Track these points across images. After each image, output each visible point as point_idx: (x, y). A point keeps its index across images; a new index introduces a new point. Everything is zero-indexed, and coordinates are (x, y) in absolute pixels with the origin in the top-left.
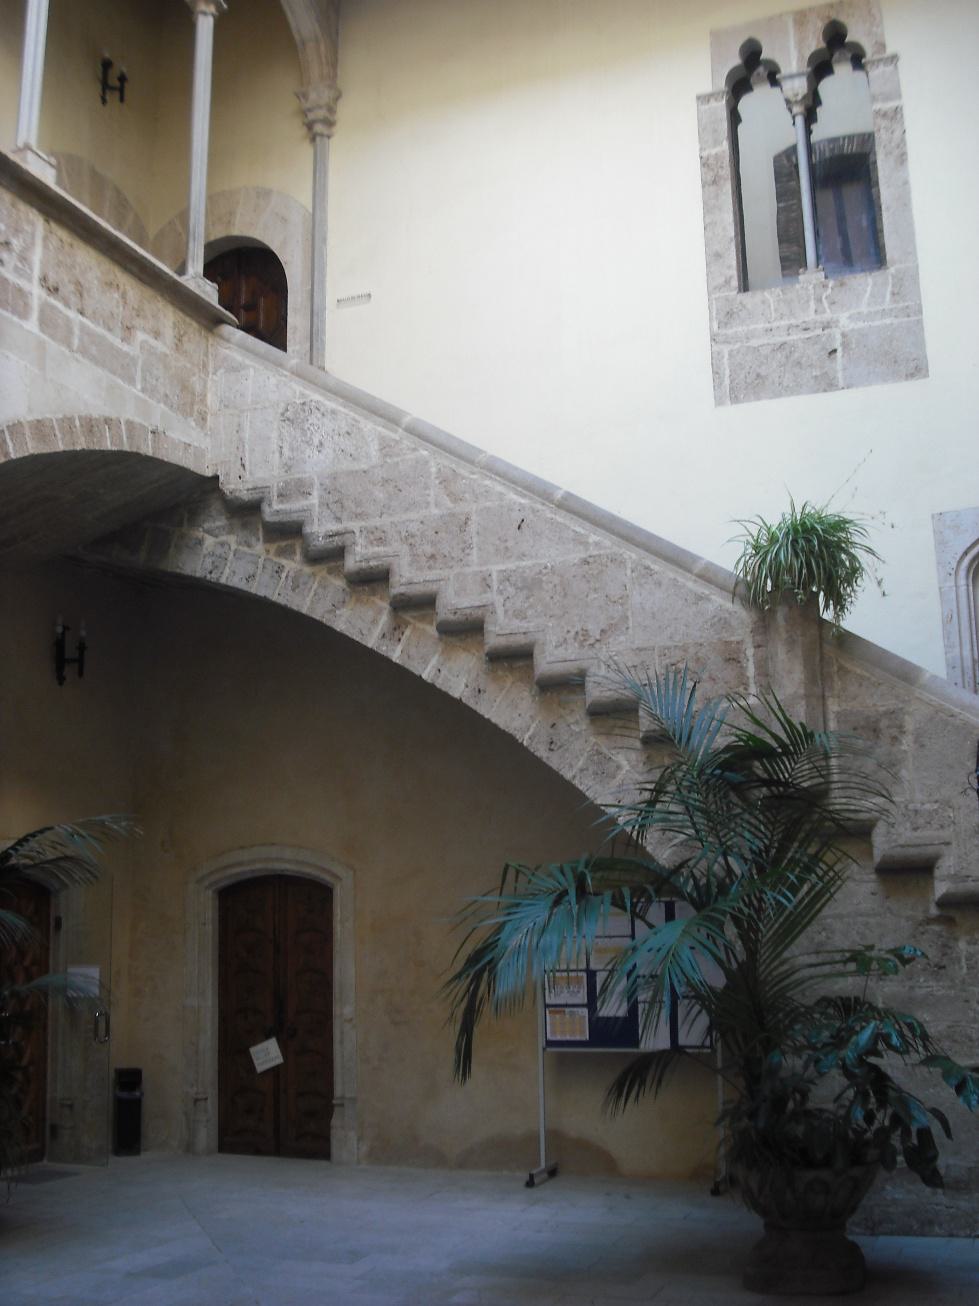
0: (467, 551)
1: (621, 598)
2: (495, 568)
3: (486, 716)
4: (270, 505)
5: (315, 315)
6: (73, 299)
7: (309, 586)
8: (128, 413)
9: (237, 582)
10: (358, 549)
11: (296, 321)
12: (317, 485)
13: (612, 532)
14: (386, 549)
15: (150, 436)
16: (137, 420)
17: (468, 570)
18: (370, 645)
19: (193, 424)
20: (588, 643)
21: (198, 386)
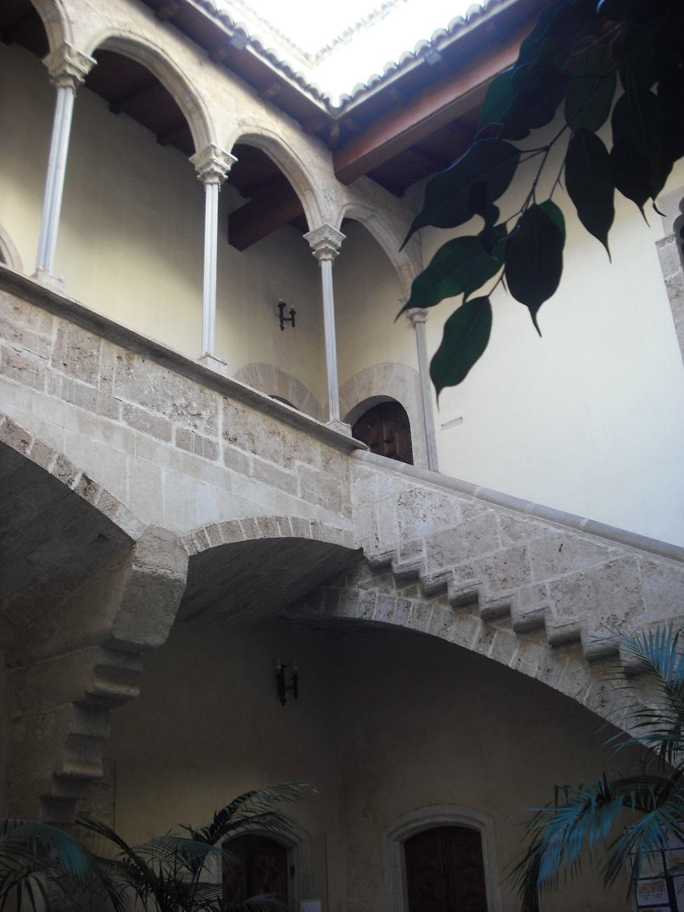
0: (527, 573)
1: (636, 588)
2: (547, 582)
3: (555, 688)
4: (396, 563)
5: (429, 437)
6: (247, 444)
7: (427, 614)
8: (294, 513)
9: (382, 618)
10: (455, 583)
11: (417, 443)
12: (425, 544)
13: (624, 542)
14: (473, 580)
15: (311, 526)
16: (300, 516)
17: (529, 586)
18: (471, 649)
19: (342, 516)
20: (617, 624)
21: (343, 492)
